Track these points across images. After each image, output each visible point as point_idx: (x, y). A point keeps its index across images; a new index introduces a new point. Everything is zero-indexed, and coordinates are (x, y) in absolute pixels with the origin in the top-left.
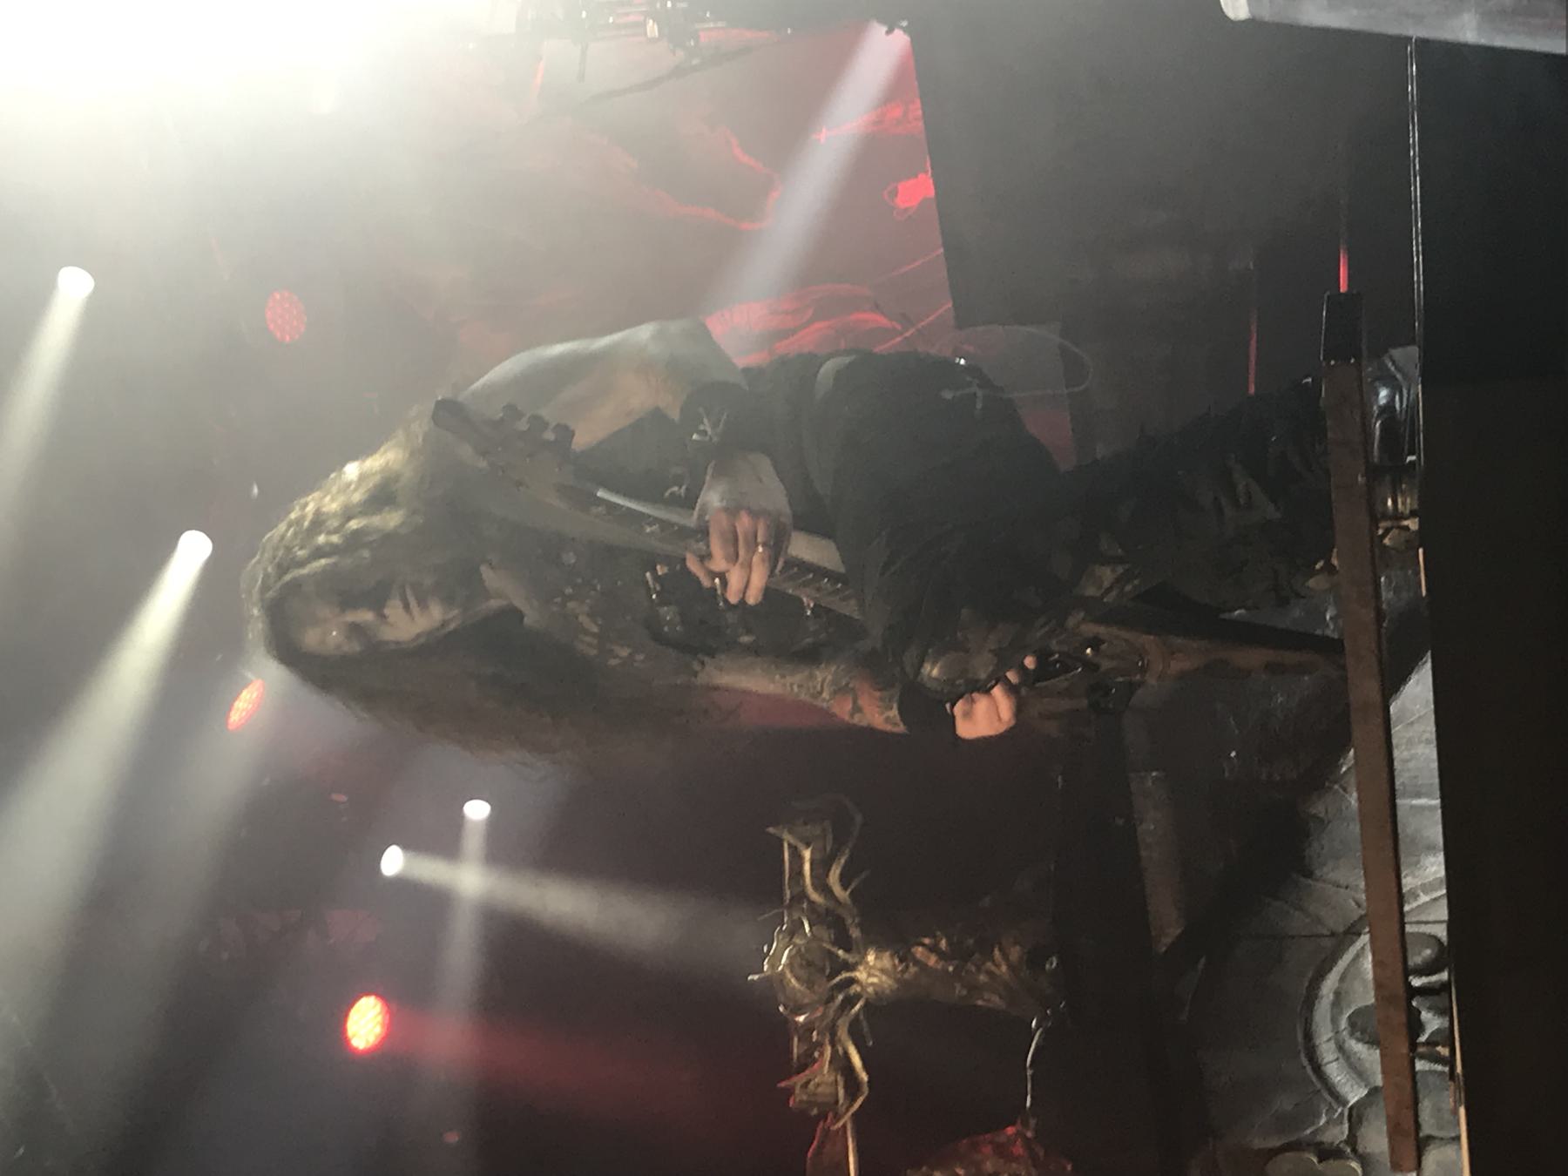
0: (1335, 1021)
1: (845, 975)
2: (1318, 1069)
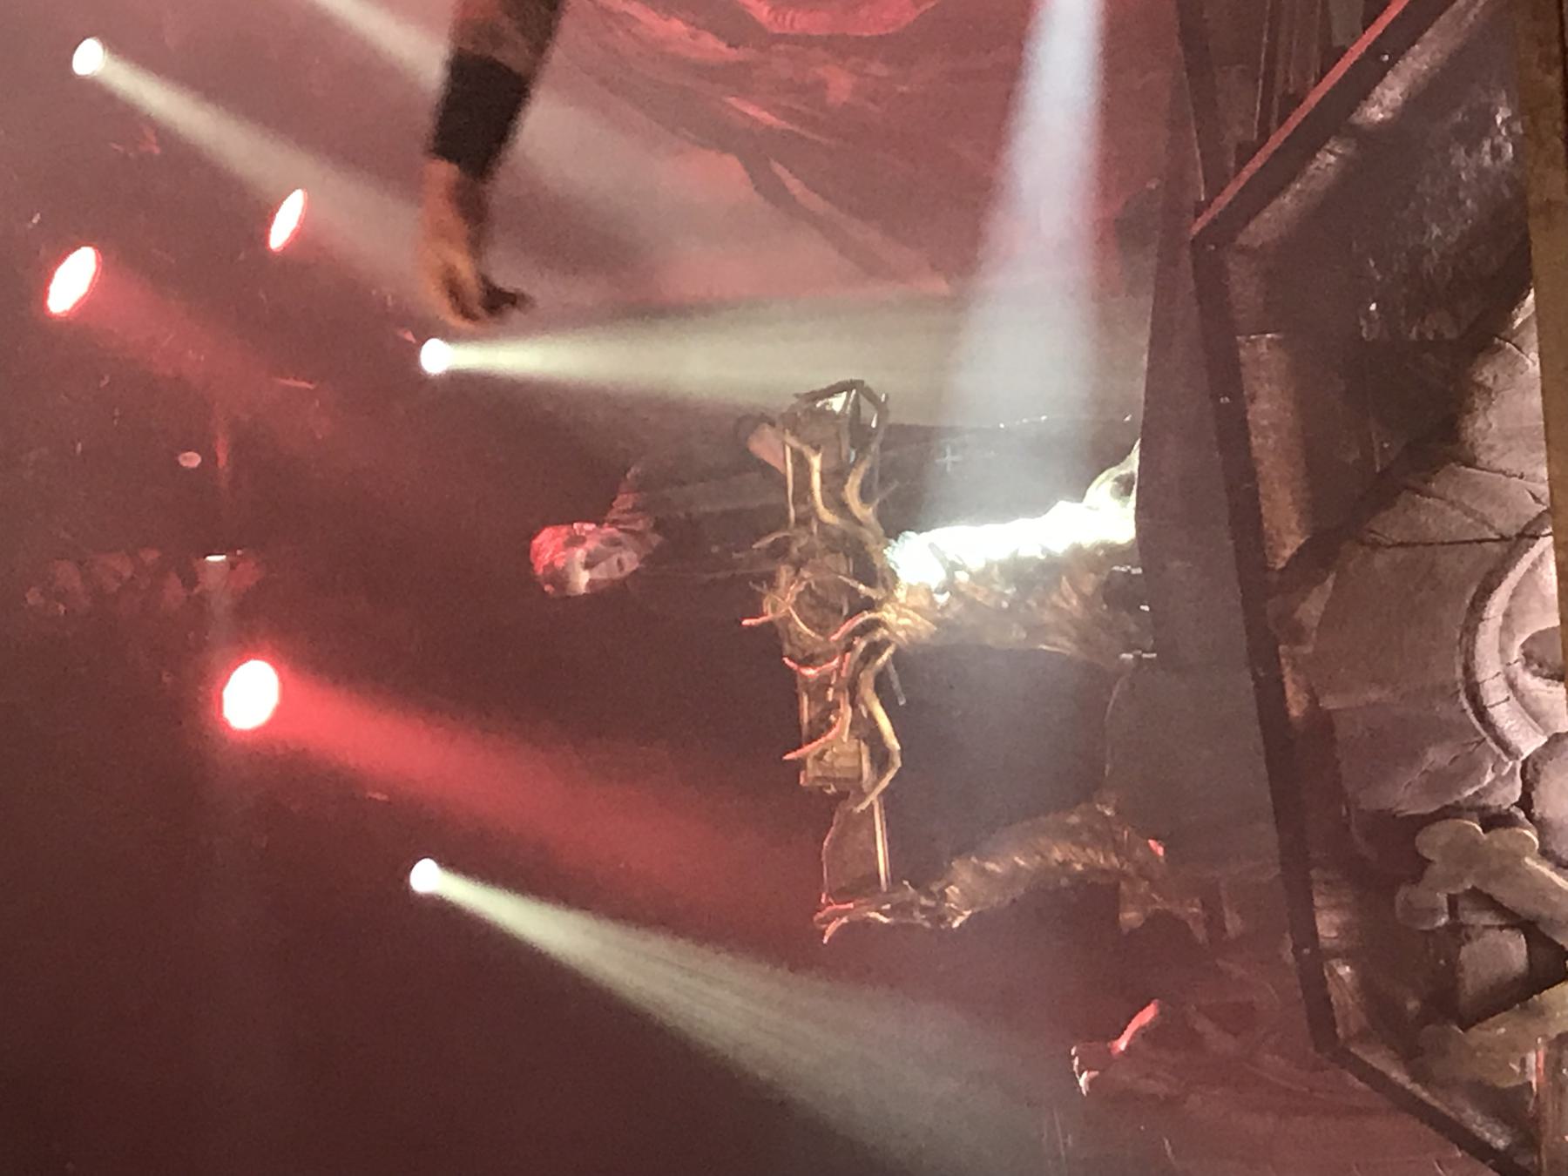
1: (867, 616)
2: (1481, 713)
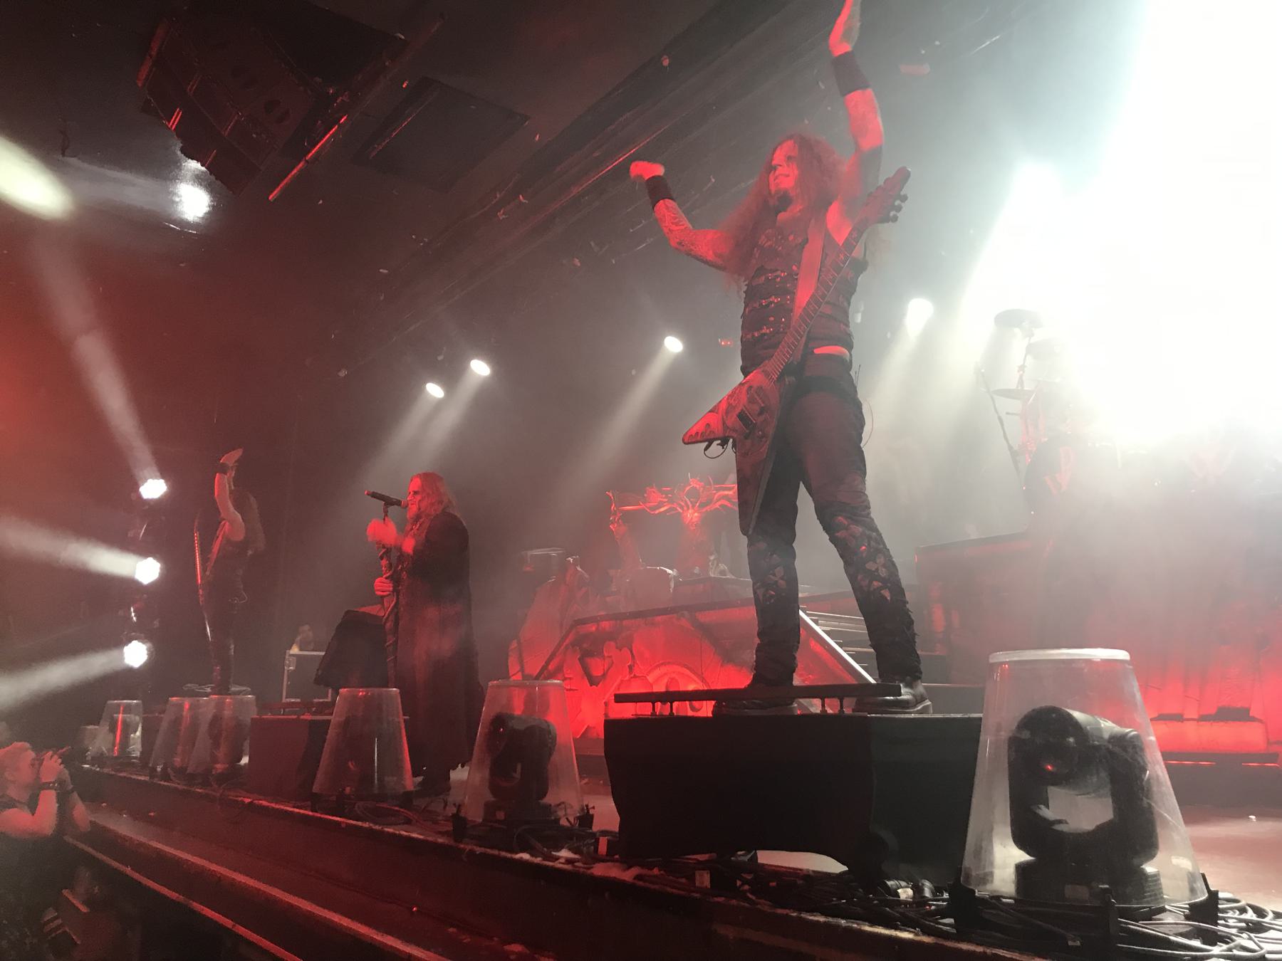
2: (658, 666)
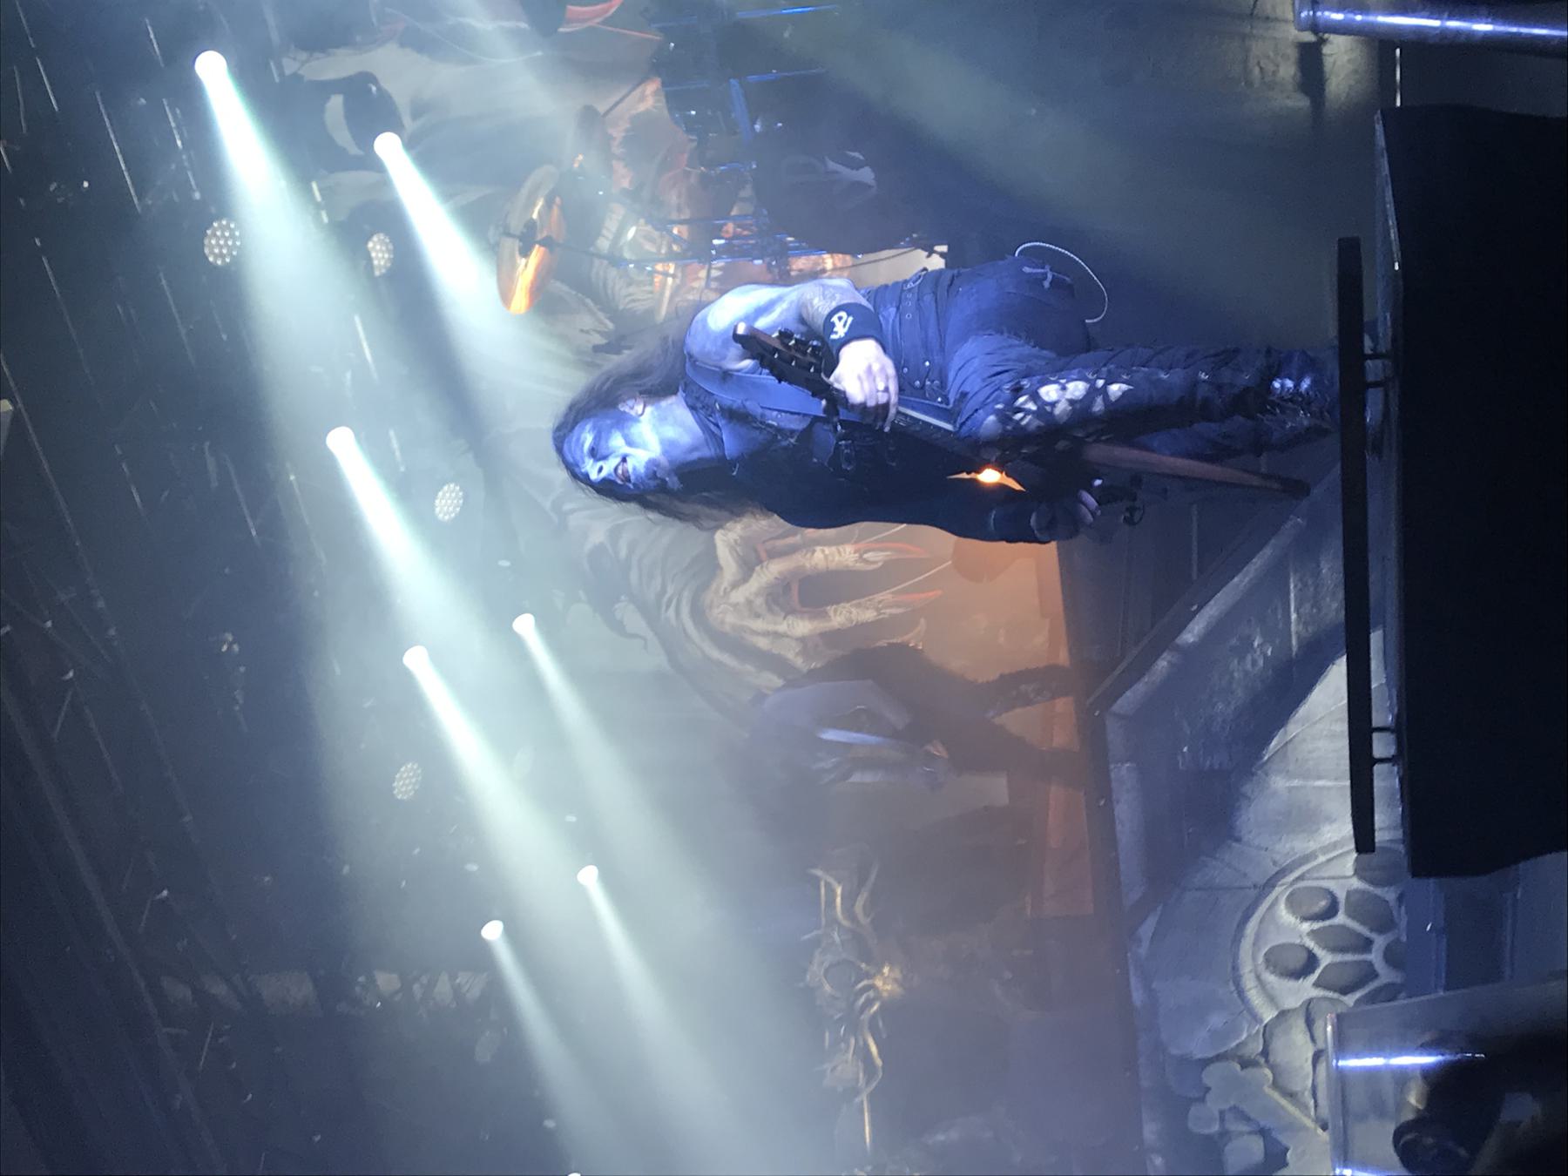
0: (1254, 958)
1: (865, 982)
2: (1241, 993)
